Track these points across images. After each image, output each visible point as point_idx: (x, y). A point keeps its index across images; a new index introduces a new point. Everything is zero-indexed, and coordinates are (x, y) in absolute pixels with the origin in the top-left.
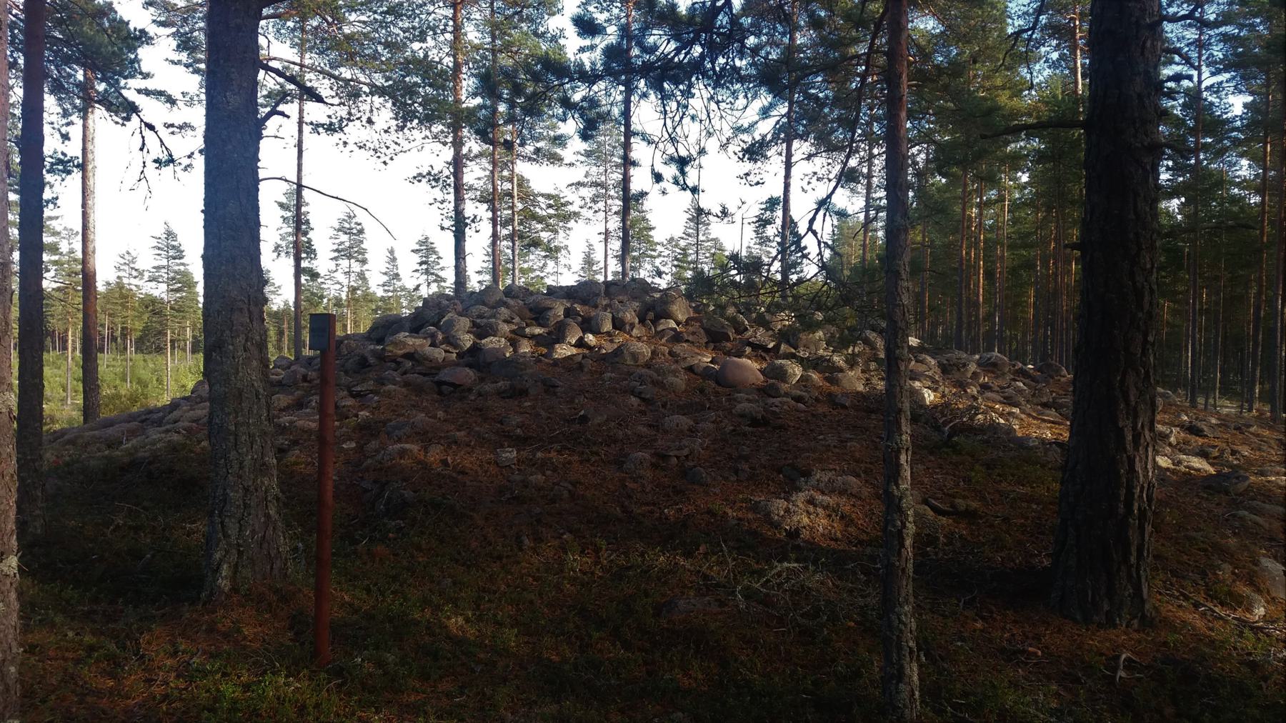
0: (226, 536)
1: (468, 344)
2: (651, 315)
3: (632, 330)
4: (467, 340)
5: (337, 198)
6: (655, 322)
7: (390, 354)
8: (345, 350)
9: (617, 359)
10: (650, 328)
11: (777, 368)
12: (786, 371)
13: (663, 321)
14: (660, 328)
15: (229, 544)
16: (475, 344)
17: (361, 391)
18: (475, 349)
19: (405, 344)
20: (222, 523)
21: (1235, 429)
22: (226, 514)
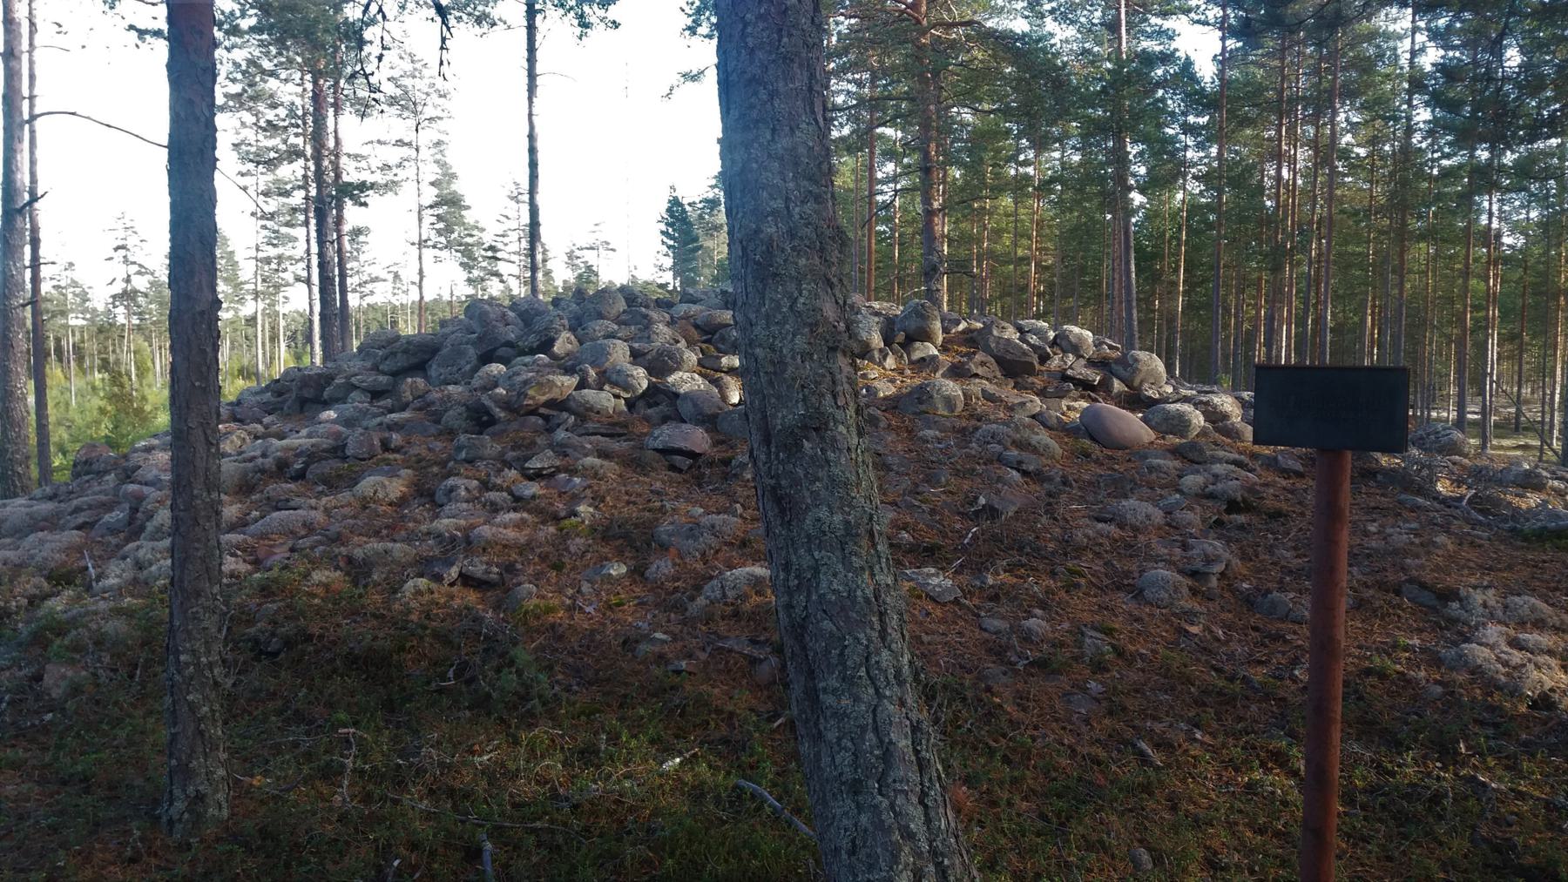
0: (909, 836)
1: (645, 385)
2: (901, 337)
3: (885, 359)
4: (641, 379)
5: (88, 118)
6: (907, 344)
7: (531, 402)
8: (408, 394)
9: (923, 407)
10: (902, 356)
11: (1173, 418)
12: (1189, 421)
13: (918, 344)
14: (917, 355)
15: (918, 854)
16: (651, 386)
17: (543, 469)
18: (653, 390)
19: (552, 384)
20: (892, 806)
21: (381, 441)
22: (899, 787)
